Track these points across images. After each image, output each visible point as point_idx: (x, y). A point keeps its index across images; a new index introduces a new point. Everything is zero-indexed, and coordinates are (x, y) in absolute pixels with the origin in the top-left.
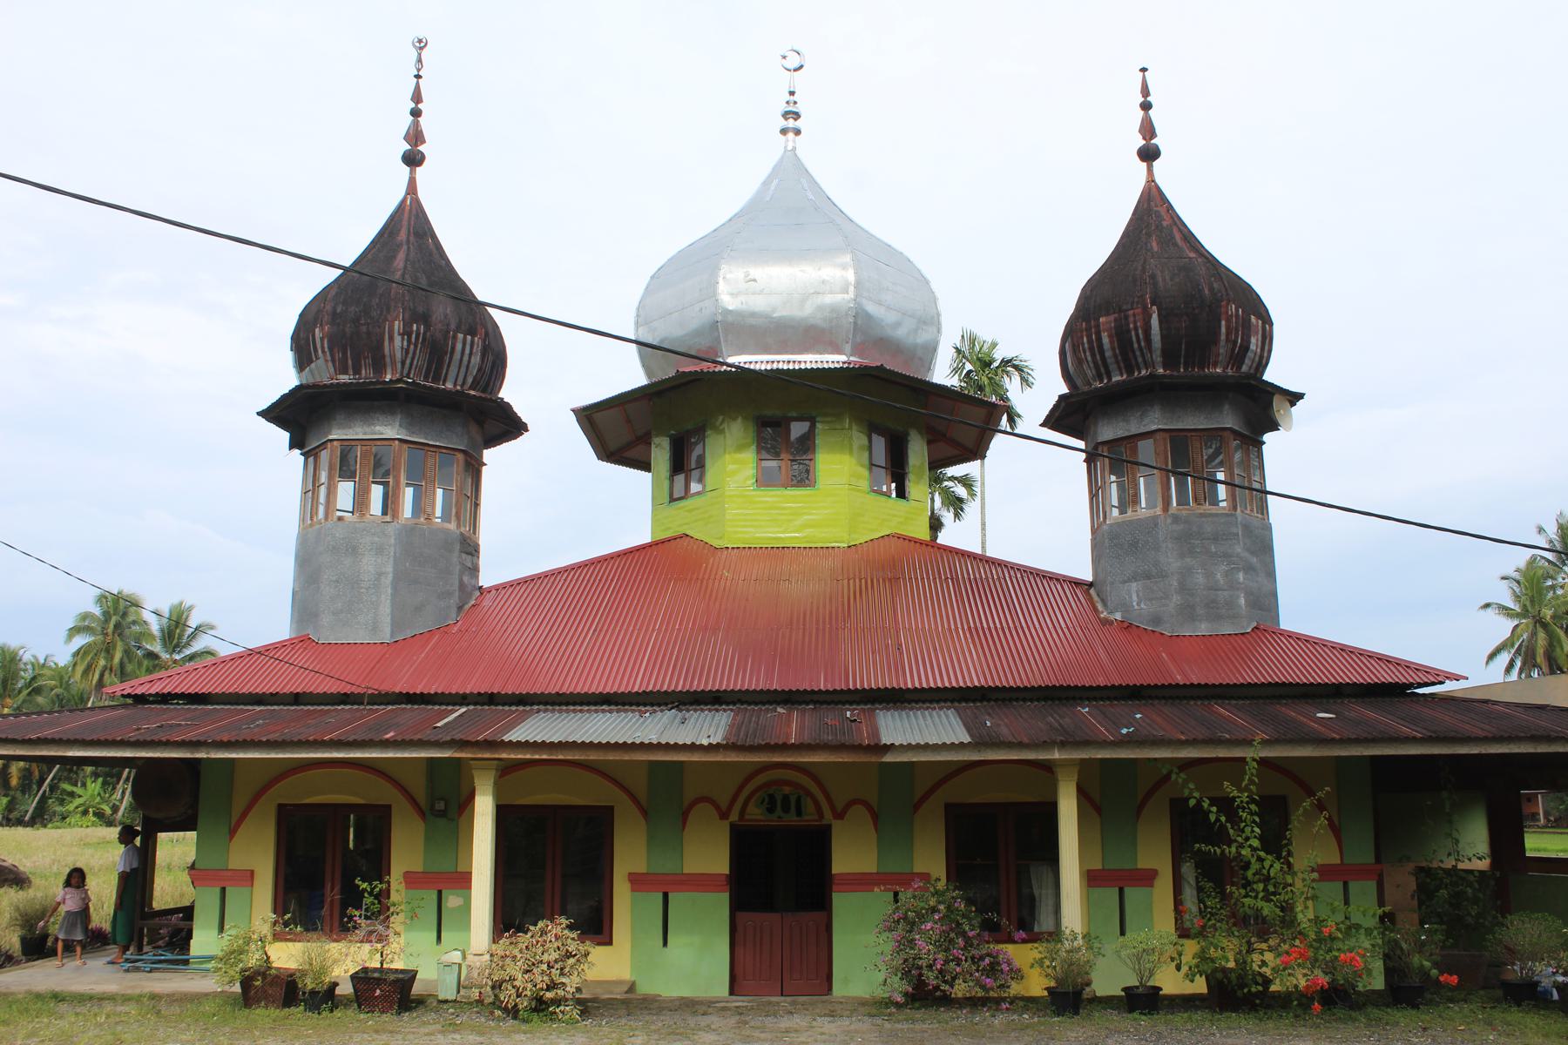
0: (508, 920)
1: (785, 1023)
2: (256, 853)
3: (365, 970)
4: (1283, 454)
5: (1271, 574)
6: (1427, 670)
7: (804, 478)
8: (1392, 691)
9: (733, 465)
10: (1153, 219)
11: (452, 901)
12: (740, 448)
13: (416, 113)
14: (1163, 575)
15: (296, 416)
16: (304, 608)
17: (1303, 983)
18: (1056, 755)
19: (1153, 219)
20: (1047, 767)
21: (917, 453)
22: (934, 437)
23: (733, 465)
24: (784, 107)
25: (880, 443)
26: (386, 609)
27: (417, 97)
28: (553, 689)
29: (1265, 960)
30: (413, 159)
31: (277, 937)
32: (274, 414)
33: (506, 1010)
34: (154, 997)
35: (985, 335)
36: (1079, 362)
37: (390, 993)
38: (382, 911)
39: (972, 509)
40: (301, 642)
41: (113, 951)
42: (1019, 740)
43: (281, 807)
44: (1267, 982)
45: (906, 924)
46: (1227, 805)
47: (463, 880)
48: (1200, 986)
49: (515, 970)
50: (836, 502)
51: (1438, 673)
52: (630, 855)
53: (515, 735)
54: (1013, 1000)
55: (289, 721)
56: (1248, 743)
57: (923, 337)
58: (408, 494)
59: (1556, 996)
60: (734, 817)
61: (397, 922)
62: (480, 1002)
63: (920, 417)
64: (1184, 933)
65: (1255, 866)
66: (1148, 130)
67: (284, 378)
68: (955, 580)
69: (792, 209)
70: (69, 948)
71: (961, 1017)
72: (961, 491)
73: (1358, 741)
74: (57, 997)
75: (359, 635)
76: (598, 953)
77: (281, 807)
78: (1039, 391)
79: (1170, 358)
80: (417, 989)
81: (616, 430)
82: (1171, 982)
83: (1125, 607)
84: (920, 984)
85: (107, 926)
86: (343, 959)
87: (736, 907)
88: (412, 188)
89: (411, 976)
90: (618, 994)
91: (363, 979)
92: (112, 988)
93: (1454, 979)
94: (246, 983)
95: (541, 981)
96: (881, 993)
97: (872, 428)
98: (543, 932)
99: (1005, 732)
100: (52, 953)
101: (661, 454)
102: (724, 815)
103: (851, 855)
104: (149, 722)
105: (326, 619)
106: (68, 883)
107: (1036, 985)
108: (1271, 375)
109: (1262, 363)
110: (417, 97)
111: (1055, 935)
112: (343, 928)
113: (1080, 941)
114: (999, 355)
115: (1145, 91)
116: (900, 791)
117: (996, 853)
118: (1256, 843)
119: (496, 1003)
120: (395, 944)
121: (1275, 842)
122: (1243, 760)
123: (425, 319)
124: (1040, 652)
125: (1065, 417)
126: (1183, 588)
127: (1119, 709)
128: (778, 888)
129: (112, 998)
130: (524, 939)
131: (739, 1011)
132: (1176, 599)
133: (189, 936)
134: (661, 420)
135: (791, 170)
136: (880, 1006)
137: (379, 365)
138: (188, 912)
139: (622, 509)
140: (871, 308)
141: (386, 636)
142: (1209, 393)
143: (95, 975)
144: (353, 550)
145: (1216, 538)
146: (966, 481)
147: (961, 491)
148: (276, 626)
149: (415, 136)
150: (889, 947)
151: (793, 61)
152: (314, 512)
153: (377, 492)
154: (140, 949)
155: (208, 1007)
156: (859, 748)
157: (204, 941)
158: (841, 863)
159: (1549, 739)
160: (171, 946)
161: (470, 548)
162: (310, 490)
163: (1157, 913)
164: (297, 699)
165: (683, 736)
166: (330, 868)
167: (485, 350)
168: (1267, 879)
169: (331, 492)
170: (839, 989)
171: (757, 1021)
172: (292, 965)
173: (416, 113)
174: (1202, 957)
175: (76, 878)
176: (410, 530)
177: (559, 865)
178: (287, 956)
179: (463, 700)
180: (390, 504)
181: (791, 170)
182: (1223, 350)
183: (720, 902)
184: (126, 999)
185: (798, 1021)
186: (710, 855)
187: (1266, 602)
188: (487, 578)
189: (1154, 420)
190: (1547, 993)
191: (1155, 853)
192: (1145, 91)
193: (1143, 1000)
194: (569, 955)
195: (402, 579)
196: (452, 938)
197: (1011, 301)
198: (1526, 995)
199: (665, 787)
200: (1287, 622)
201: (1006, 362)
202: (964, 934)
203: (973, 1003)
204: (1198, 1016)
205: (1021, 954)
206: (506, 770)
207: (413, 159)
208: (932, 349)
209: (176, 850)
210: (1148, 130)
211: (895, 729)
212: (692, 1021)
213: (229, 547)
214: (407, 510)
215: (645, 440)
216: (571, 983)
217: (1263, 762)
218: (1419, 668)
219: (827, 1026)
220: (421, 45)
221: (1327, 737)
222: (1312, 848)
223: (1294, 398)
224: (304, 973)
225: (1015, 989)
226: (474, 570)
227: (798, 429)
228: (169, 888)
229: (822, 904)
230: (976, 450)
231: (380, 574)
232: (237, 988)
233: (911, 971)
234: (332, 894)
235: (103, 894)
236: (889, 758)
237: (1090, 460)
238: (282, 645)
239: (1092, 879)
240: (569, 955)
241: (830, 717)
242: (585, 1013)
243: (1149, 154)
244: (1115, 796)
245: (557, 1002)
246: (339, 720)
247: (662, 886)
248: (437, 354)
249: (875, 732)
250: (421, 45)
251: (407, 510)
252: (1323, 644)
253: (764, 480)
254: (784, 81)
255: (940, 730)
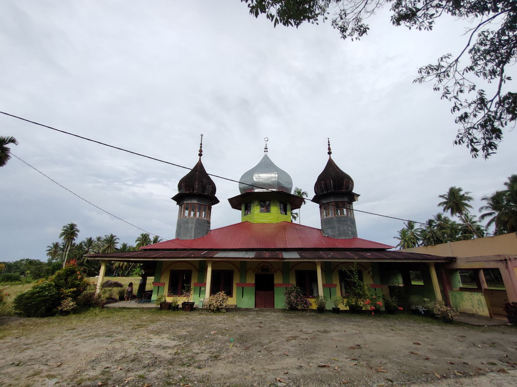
0: (213, 292)
1: (266, 313)
2: (166, 280)
3: (185, 302)
4: (355, 205)
5: (355, 228)
6: (388, 246)
7: (268, 211)
8: (382, 250)
9: (256, 209)
10: (331, 165)
11: (203, 289)
12: (257, 206)
13: (201, 147)
14: (335, 228)
15: (178, 199)
16: (178, 233)
17: (369, 308)
18: (317, 260)
19: (331, 165)
20: (315, 264)
21: (289, 207)
22: (292, 204)
23: (256, 209)
24: (264, 147)
25: (282, 205)
26: (193, 234)
27: (201, 144)
28: (223, 248)
29: (361, 303)
30: (200, 155)
31: (168, 296)
32: (174, 198)
33: (211, 310)
34: (143, 308)
35: (300, 188)
36: (318, 190)
37: (189, 307)
38: (189, 291)
39: (298, 219)
40: (177, 239)
41: (136, 299)
42: (309, 257)
43: (171, 271)
44: (362, 308)
45: (289, 293)
46: (351, 271)
47: (205, 285)
48: (348, 308)
49: (214, 302)
50: (274, 215)
51: (391, 246)
52: (236, 281)
53: (215, 256)
54: (310, 310)
55: (174, 253)
56: (355, 259)
57: (289, 187)
58: (198, 213)
59: (423, 313)
60: (256, 272)
61: (192, 292)
62: (206, 309)
63: (289, 200)
64: (344, 297)
65: (358, 283)
66: (329, 149)
67: (176, 192)
68: (296, 229)
69: (266, 165)
70: (128, 299)
71: (300, 313)
72: (296, 216)
73: (376, 259)
74: (124, 308)
75: (188, 238)
76: (230, 299)
77: (171, 271)
78: (312, 194)
79: (334, 189)
80: (194, 306)
81: (235, 203)
82: (342, 307)
83: (328, 234)
84: (291, 306)
85: (136, 294)
86: (181, 300)
87: (256, 290)
88: (200, 159)
89: (193, 303)
90: (233, 307)
91: (184, 304)
92: (135, 306)
93: (402, 309)
94: (161, 305)
95: (219, 304)
96: (284, 308)
97: (281, 202)
98: (219, 294)
99: (307, 256)
100: (125, 300)
101: (243, 208)
102: (254, 272)
103: (278, 280)
104: (147, 254)
105: (182, 235)
106: (129, 286)
107: (314, 307)
108: (353, 191)
109: (352, 189)
110: (201, 144)
111: (318, 296)
112: (181, 294)
113: (323, 298)
114: (302, 192)
115: (329, 142)
116: (287, 267)
117: (305, 281)
118: (357, 279)
119: (210, 309)
120: (191, 297)
121: (361, 279)
122: (354, 262)
123: (202, 182)
124: (312, 242)
125: (315, 200)
126: (338, 230)
127: (328, 252)
128: (264, 289)
129: (134, 308)
130: (216, 296)
131: (257, 311)
132: (337, 232)
133: (151, 296)
134: (243, 201)
135: (266, 158)
136: (283, 310)
137: (193, 190)
138: (152, 291)
139: (236, 216)
140: (280, 181)
141: (193, 238)
142: (343, 195)
143: (132, 304)
144: (187, 222)
145: (344, 221)
146: (296, 214)
147: (296, 216)
148: (172, 236)
149: (201, 151)
150: (285, 298)
151: (266, 139)
152: (181, 216)
153: (192, 213)
154: (142, 299)
155: (153, 310)
156: (279, 259)
157: (154, 297)
158: (276, 282)
159: (416, 259)
160: (148, 298)
161: (209, 223)
162: (180, 212)
163: (338, 293)
164: (175, 250)
165: (247, 256)
166: (180, 283)
167: (212, 188)
168: (360, 286)
169: (184, 212)
170: (276, 307)
171: (260, 313)
172: (171, 301)
173: (201, 147)
174: (348, 302)
175: (131, 285)
176: (198, 219)
177: (223, 283)
178: (169, 300)
179: (206, 250)
180: (195, 215)
181: (266, 158)
182: (344, 187)
183: (253, 288)
184: (137, 308)
185: (268, 313)
186: (251, 280)
187: (355, 233)
188: (211, 228)
189: (332, 200)
190: (421, 312)
191: (336, 281)
192: (329, 142)
193: (336, 311)
194: (224, 299)
195: (196, 228)
196: (202, 297)
197: (304, 180)
198: (416, 312)
199: (243, 266)
200: (359, 237)
201: (303, 193)
202: (300, 296)
203: (302, 310)
204: (348, 314)
205: (312, 301)
206: (214, 263)
207: (200, 155)
208: (291, 189)
209: (150, 280)
210: (329, 149)
211: (286, 255)
212: (248, 313)
213: (162, 221)
214: (198, 216)
215: (240, 205)
216: (224, 305)
217: (358, 263)
218: (387, 246)
219: (273, 314)
220: (202, 135)
221: (369, 258)
222: (368, 282)
223: (358, 195)
224: (172, 303)
225: (310, 307)
226: (209, 227)
227: (268, 203)
228: (149, 287)
229: (272, 289)
230: (299, 207)
231: (192, 227)
232: (159, 306)
233: (290, 303)
234: (180, 287)
235: (136, 288)
236: (285, 261)
237: (320, 207)
238: (173, 240)
239: (324, 285)
240: (224, 299)
241: (274, 253)
242: (227, 311)
243: (330, 153)
244: (328, 269)
245: (222, 308)
246: (186, 254)
247: (243, 287)
248: (204, 188)
249: (282, 256)
250: (202, 135)
251: (198, 216)
252: (367, 241)
253: (261, 211)
254: (265, 143)
255: (295, 256)
